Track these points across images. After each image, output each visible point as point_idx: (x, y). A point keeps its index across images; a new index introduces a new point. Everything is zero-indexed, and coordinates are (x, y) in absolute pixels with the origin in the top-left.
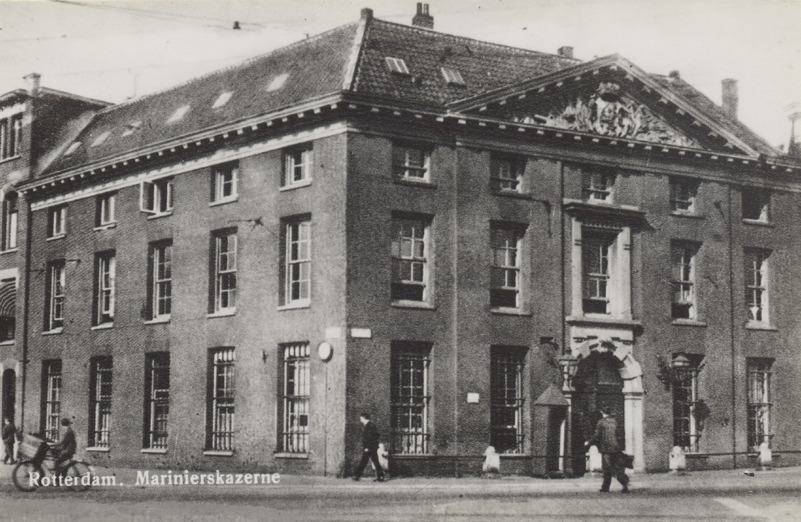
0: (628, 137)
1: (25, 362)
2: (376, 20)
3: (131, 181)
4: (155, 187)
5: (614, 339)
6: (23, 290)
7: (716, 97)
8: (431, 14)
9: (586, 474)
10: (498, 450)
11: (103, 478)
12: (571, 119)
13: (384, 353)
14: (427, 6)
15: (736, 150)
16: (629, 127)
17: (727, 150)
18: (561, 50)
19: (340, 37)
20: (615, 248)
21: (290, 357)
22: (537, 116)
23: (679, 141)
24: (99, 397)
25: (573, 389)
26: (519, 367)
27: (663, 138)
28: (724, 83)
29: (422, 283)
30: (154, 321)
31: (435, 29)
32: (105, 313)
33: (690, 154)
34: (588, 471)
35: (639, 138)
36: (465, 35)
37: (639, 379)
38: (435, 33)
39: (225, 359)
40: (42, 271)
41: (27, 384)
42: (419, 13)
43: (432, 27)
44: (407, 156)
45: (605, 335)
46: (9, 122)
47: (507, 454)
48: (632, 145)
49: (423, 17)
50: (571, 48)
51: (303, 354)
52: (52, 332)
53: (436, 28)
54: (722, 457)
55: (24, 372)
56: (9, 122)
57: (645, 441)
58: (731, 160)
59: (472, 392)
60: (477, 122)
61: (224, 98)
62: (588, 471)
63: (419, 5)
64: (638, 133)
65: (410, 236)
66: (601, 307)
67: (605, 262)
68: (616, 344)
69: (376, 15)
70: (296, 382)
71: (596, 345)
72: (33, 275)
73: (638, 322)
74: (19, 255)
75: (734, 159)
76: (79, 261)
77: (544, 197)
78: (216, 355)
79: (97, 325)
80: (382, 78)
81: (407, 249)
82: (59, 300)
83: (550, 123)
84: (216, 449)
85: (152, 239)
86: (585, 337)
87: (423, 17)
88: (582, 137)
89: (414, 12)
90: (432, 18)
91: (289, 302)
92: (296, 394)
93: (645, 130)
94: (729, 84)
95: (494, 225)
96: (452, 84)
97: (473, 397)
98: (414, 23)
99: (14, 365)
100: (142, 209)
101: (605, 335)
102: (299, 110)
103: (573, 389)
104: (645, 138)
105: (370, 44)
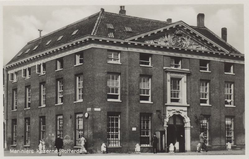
0: (185, 47)
2: (105, 12)
4: (58, 62)
5: (180, 110)
6: (6, 98)
7: (219, 35)
8: (125, 10)
9: (169, 152)
10: (140, 144)
12: (166, 42)
13: (104, 117)
15: (221, 51)
16: (186, 44)
18: (167, 20)
20: (181, 82)
21: (78, 117)
22: (154, 41)
23: (203, 49)
27: (197, 47)
30: (42, 107)
31: (126, 15)
32: (29, 102)
33: (206, 52)
34: (170, 151)
36: (136, 16)
37: (189, 123)
38: (126, 16)
39: (80, 116)
41: (8, 127)
42: (121, 9)
44: (113, 55)
45: (178, 109)
47: (144, 146)
49: (122, 10)
51: (81, 116)
52: (28, 108)
54: (217, 146)
57: (191, 142)
58: (220, 54)
59: (134, 127)
60: (141, 44)
61: (74, 33)
62: (170, 151)
65: (114, 80)
66: (177, 101)
68: (181, 111)
69: (105, 11)
70: (80, 125)
71: (175, 112)
73: (189, 105)
75: (221, 53)
78: (77, 115)
79: (26, 108)
82: (16, 100)
83: (159, 44)
85: (40, 82)
86: (171, 110)
87: (122, 10)
88: (170, 47)
89: (120, 9)
90: (125, 11)
91: (78, 100)
92: (80, 128)
94: (224, 31)
96: (128, 32)
97: (134, 129)
100: (37, 73)
103: (167, 126)
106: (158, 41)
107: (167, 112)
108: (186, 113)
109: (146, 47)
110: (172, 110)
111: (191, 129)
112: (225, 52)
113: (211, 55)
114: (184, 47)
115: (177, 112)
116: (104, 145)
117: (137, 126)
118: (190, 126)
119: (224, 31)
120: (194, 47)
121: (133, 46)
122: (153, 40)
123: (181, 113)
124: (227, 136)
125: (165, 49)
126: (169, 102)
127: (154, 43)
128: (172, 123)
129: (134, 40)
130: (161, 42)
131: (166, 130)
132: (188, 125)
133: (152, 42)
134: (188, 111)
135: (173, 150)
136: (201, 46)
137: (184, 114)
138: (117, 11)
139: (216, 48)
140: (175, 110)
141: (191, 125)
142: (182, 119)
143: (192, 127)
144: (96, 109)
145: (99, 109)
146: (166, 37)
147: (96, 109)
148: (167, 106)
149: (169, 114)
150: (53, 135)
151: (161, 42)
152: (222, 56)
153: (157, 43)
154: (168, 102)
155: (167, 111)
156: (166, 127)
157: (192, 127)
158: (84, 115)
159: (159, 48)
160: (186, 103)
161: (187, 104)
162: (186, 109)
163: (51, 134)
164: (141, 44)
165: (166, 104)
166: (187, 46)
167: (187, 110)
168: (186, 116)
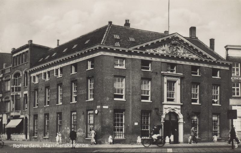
1: (30, 115)
3: (52, 68)
6: (29, 97)
7: (208, 44)
10: (141, 137)
11: (36, 145)
12: (163, 50)
14: (128, 20)
15: (210, 58)
16: (180, 53)
17: (207, 58)
19: (105, 28)
21: (89, 113)
22: (162, 49)
23: (195, 57)
24: (47, 124)
25: (164, 121)
26: (150, 114)
27: (189, 55)
28: (210, 40)
29: (197, 99)
30: (59, 104)
35: (183, 55)
36: (142, 29)
40: (33, 92)
43: (129, 27)
45: (173, 107)
46: (22, 54)
48: (180, 57)
49: (127, 24)
50: (214, 39)
53: (130, 27)
55: (29, 118)
56: (22, 54)
60: (142, 52)
63: (126, 21)
64: (183, 54)
66: (172, 100)
67: (174, 88)
68: (175, 109)
69: (113, 23)
72: (31, 93)
74: (28, 88)
76: (41, 89)
77: (156, 71)
80: (112, 40)
81: (193, 92)
84: (89, 138)
87: (127, 24)
89: (125, 23)
92: (91, 123)
93: (184, 53)
94: (212, 41)
95: (142, 79)
97: (136, 124)
98: (124, 26)
99: (27, 116)
101: (173, 107)
102: (93, 48)
104: (185, 55)
105: (111, 31)
106: (157, 50)
107: (164, 110)
108: (180, 110)
109: (147, 55)
110: (168, 108)
111: (184, 124)
112: (212, 59)
113: (201, 62)
114: (178, 55)
115: (173, 109)
116: (110, 137)
117: (139, 121)
118: (183, 122)
119: (212, 41)
120: (187, 55)
121: (135, 53)
122: (153, 49)
123: (176, 111)
124: (213, 130)
125: (162, 56)
126: (165, 101)
127: (153, 52)
128: (168, 119)
129: (136, 49)
130: (159, 51)
131: (163, 125)
132: (181, 121)
133: (152, 51)
134: (181, 109)
135: (169, 142)
136: (192, 54)
137: (178, 112)
138: (122, 24)
139: (206, 56)
140: (170, 108)
141: (184, 121)
142: (176, 115)
143: (185, 122)
144: (104, 107)
145: (107, 107)
146: (163, 46)
147: (104, 107)
148: (164, 104)
149: (166, 111)
150: (68, 128)
151: (159, 51)
152: (210, 63)
153: (156, 51)
154: (164, 101)
155: (164, 109)
156: (163, 122)
157: (185, 122)
158: (94, 111)
159: (157, 56)
160: (180, 102)
161: (181, 103)
162: (179, 107)
163: (67, 127)
164: (142, 52)
165: (163, 103)
166: (181, 54)
167: (180, 108)
168: (180, 113)
